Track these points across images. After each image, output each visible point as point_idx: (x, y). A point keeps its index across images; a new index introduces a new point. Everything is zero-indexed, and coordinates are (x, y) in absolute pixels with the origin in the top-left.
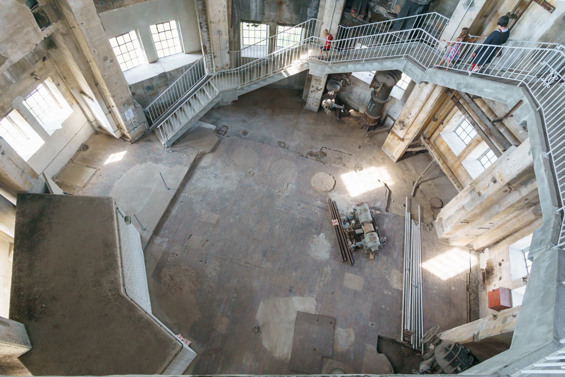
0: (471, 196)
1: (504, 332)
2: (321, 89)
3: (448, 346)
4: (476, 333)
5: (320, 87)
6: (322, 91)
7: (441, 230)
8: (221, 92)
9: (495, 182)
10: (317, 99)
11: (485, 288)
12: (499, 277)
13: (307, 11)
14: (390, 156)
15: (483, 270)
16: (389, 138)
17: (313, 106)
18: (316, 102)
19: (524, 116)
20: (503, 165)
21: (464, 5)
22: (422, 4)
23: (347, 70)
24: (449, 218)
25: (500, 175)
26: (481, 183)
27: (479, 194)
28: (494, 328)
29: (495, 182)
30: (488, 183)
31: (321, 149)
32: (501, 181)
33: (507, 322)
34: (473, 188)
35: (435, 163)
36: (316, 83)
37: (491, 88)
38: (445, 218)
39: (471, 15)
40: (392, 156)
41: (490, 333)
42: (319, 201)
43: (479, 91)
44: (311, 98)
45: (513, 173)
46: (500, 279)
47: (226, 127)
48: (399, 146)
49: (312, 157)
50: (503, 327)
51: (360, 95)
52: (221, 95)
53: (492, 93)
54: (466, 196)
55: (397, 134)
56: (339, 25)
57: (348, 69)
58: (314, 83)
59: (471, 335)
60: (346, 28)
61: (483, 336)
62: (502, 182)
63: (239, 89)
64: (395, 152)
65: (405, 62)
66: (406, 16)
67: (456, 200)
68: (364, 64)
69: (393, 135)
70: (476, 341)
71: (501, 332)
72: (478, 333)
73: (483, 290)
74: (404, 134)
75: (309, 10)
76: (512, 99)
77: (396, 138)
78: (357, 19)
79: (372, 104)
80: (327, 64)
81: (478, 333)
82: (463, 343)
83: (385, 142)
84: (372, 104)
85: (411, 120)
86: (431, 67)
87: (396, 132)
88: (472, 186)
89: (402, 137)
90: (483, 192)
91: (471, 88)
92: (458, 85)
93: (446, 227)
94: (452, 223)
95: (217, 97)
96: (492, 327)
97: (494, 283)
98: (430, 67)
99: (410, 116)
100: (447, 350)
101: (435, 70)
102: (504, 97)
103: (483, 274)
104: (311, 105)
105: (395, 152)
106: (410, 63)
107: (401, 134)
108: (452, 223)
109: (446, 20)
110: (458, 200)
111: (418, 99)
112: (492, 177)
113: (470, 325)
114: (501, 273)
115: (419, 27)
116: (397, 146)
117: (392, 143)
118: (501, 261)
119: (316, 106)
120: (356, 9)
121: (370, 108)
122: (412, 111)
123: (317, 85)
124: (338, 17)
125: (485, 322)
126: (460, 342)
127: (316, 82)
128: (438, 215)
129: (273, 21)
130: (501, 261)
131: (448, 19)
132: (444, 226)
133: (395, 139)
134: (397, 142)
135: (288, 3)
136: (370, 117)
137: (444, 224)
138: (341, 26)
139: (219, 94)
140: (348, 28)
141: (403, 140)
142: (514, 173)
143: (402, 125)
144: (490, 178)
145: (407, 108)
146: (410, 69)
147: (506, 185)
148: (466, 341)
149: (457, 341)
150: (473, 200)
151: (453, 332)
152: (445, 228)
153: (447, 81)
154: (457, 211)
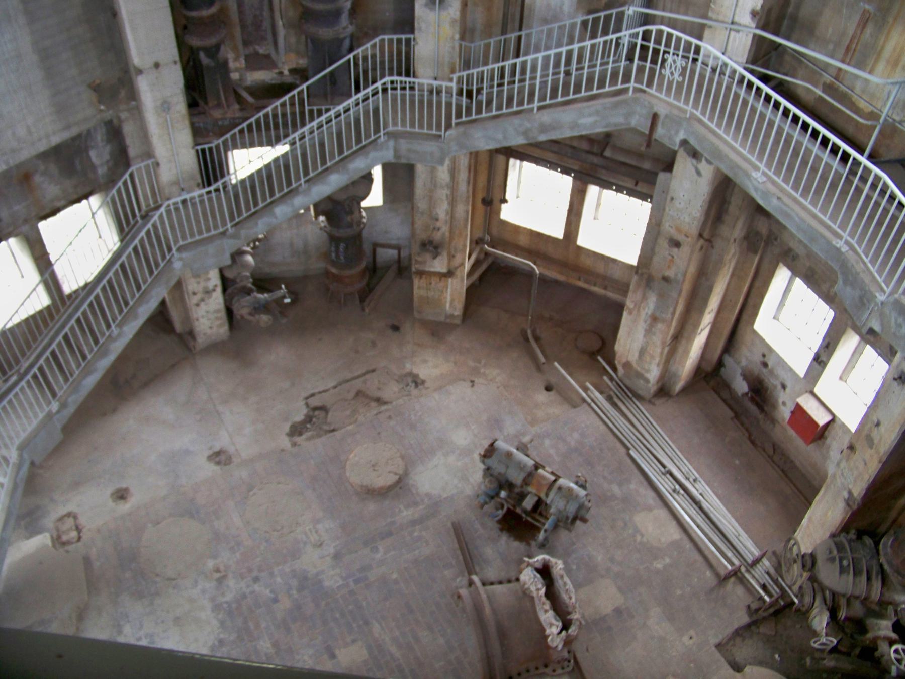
0: (653, 291)
1: (884, 459)
2: (216, 286)
3: (828, 552)
4: (846, 495)
5: (211, 285)
6: (219, 290)
7: (642, 382)
8: (21, 448)
9: (677, 244)
10: (218, 311)
11: (773, 421)
12: (779, 387)
13: (89, 158)
14: (442, 319)
15: (747, 394)
16: (419, 288)
17: (215, 330)
18: (217, 319)
19: (677, 132)
20: (670, 212)
21: (426, 5)
22: (346, 34)
23: (274, 220)
24: (642, 352)
25: (678, 230)
26: (656, 259)
27: (666, 279)
28: (866, 464)
29: (677, 244)
30: (667, 253)
31: (307, 405)
32: (686, 239)
33: (876, 441)
34: (645, 276)
35: (543, 280)
36: (198, 283)
37: (590, 115)
38: (633, 357)
39: (450, 14)
40: (447, 317)
41: (866, 477)
42: (402, 512)
43: (572, 128)
44: (203, 317)
45: (696, 215)
46: (784, 387)
47: (69, 515)
48: (449, 290)
49: (304, 436)
50: (877, 452)
51: (291, 245)
52: (25, 456)
53: (596, 122)
54: (644, 298)
55: (432, 269)
56: (193, 148)
57: (276, 218)
58: (195, 285)
59: (841, 505)
60: (213, 145)
61: (858, 490)
62: (689, 239)
63: (58, 412)
64: (448, 305)
65: (391, 143)
66: (330, 65)
67: (630, 313)
68: (309, 189)
69: (424, 276)
70: (855, 507)
71: (880, 462)
72: (850, 493)
73: (774, 426)
74: (446, 261)
75: (93, 154)
76: (637, 117)
77: (434, 280)
78: (225, 119)
79: (337, 248)
80: (224, 234)
81: (850, 493)
82: (840, 528)
83: (416, 299)
84: (337, 248)
85: (445, 229)
86: (448, 126)
87: (427, 269)
88: (642, 274)
89: (445, 270)
90: (670, 273)
91: (554, 128)
92: (525, 133)
93: (648, 371)
94: (652, 357)
95: (19, 467)
96: (861, 466)
97: (780, 401)
98: (446, 130)
99: (438, 224)
100: (832, 560)
101: (461, 129)
102: (621, 120)
103: (752, 400)
104: (209, 331)
105: (448, 305)
106: (402, 141)
107: (439, 265)
108: (652, 357)
109: (408, 41)
110: (635, 312)
111: (435, 186)
112: (667, 241)
113: (825, 492)
114: (777, 377)
115: (383, 76)
116: (447, 292)
117: (431, 294)
118: (762, 359)
119: (220, 326)
120: (216, 102)
121: (338, 256)
122: (437, 214)
123: (203, 284)
124: (184, 137)
125: (845, 468)
126: (834, 531)
127: (198, 279)
128: (616, 362)
129: (26, 221)
130: (762, 359)
131: (412, 36)
132: (643, 372)
133: (433, 283)
134: (442, 284)
135: (42, 168)
136: (347, 272)
137: (639, 369)
138: (199, 148)
139: (21, 456)
140: (215, 143)
141: (450, 274)
142: (698, 215)
143: (431, 249)
144: (663, 244)
145: (422, 213)
146: (409, 151)
147: (698, 240)
148: (842, 522)
149: (828, 534)
150: (661, 296)
151: (808, 526)
152: (648, 375)
153: (500, 136)
154: (649, 332)
